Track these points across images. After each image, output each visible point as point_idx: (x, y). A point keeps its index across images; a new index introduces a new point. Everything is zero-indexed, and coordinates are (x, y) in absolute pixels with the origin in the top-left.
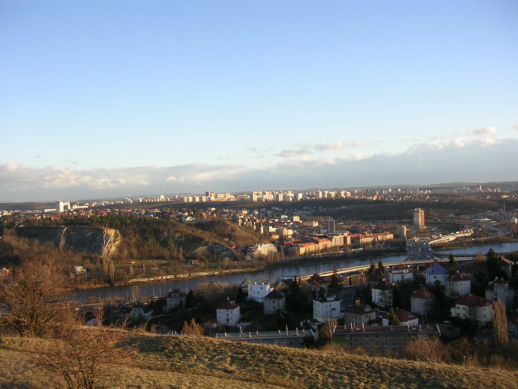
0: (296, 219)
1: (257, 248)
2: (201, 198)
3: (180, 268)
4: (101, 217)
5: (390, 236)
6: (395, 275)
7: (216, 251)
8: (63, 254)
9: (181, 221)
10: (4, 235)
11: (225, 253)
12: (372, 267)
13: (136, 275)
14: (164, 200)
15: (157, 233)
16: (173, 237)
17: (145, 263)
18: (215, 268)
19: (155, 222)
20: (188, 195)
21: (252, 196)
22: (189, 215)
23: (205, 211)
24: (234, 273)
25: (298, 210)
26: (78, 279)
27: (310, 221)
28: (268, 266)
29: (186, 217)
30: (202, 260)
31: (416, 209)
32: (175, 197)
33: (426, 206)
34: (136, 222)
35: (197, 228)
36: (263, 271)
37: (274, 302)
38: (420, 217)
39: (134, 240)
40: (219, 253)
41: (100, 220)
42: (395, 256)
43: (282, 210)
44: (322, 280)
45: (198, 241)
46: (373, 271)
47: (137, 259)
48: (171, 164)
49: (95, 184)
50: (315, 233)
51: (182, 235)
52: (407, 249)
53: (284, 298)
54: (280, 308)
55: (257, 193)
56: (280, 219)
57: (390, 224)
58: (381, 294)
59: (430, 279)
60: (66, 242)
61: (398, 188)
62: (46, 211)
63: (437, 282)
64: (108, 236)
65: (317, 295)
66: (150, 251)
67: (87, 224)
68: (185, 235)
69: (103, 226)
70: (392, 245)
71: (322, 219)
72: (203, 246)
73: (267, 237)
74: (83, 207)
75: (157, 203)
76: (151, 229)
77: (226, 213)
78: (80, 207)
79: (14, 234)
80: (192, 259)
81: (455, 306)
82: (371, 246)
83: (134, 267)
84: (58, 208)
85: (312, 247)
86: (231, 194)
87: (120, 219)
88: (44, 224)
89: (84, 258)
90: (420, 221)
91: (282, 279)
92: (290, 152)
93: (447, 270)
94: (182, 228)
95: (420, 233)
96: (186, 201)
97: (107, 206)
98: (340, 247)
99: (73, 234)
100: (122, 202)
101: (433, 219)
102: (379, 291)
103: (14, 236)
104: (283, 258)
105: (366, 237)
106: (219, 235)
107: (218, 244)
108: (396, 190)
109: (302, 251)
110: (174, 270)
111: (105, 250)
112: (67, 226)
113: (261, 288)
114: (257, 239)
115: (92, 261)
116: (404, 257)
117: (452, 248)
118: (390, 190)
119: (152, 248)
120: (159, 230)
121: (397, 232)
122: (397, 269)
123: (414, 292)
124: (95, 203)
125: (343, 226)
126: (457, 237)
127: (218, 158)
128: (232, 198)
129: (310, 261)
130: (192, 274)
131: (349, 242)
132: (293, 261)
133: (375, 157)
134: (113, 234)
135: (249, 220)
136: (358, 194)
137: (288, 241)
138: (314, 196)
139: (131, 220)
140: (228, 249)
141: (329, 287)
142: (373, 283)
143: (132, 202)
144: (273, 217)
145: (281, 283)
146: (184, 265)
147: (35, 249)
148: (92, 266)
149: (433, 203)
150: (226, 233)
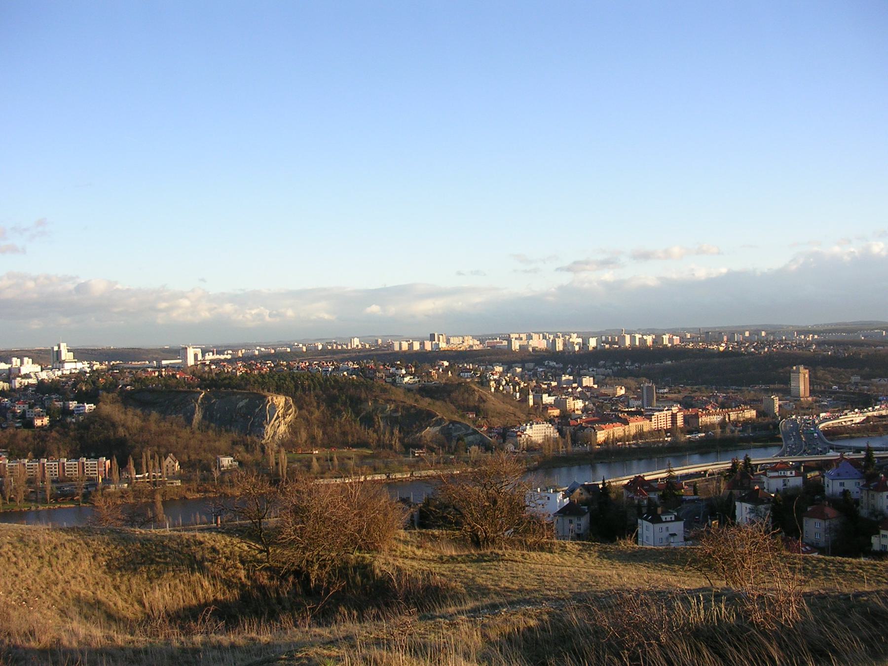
0: (588, 381)
1: (525, 430)
2: (422, 344)
3: (396, 463)
4: (260, 374)
5: (751, 414)
6: (772, 481)
7: (455, 434)
8: (199, 436)
9: (394, 383)
10: (101, 403)
11: (471, 438)
12: (735, 465)
13: (323, 473)
14: (360, 347)
15: (355, 403)
16: (383, 410)
17: (336, 453)
19: (353, 384)
20: (400, 339)
21: (510, 342)
22: (408, 374)
23: (433, 367)
25: (590, 367)
26: (227, 478)
27: (612, 385)
28: (544, 462)
29: (403, 377)
30: (431, 450)
32: (377, 341)
33: (811, 362)
34: (320, 384)
35: (422, 396)
36: (536, 469)
37: (571, 522)
38: (802, 381)
39: (317, 414)
40: (460, 439)
41: (260, 380)
42: (761, 447)
43: (561, 365)
44: (651, 486)
45: (426, 417)
46: (735, 472)
47: (323, 446)
48: (375, 284)
49: (241, 317)
50: (621, 407)
51: (397, 407)
52: (781, 436)
53: (588, 515)
54: (581, 532)
55: (517, 336)
56: (559, 382)
57: (750, 393)
58: (752, 511)
59: (833, 487)
60: (204, 417)
61: (760, 331)
62: (164, 362)
63: (845, 493)
64: (274, 407)
65: (644, 510)
66: (344, 434)
67: (238, 386)
69: (266, 390)
70: (754, 428)
71: (632, 382)
72: (434, 425)
73: (539, 413)
74: (222, 357)
75: (348, 351)
76: (347, 396)
77: (469, 371)
78: (218, 357)
79: (118, 401)
80: (414, 448)
81: (878, 533)
82: (719, 430)
83: (318, 459)
84: (185, 358)
85: (618, 430)
86: (474, 337)
87: (293, 378)
88: (166, 385)
89: (234, 443)
90: (802, 387)
91: (581, 483)
92: (587, 263)
93: (862, 473)
94: (399, 395)
95: (802, 409)
96: (397, 348)
97: (265, 357)
98: (667, 431)
99: (214, 403)
100: (289, 350)
101: (824, 384)
102: (749, 506)
103: (117, 404)
104: (570, 448)
105: (709, 414)
106: (459, 407)
107: (459, 423)
108: (757, 332)
109: (601, 436)
110: (386, 466)
111: (269, 430)
112: (205, 388)
114: (523, 417)
115: (248, 448)
116: (775, 451)
117: (858, 435)
118: (747, 334)
119: (348, 427)
120: (359, 398)
121: (762, 407)
122: (775, 468)
123: (809, 509)
124: (243, 351)
125: (669, 396)
126: (868, 417)
127: (459, 273)
128: (477, 345)
129: (616, 454)
130: (417, 474)
131: (680, 422)
132: (587, 453)
133: (730, 275)
134: (282, 404)
135: (507, 383)
136: (692, 340)
137: (576, 419)
138: (616, 343)
139: (312, 380)
140: (475, 432)
141: (660, 497)
142: (735, 492)
143: (304, 349)
144: (547, 379)
145: (578, 490)
146: (401, 458)
147: (153, 427)
148: (248, 457)
149: (824, 357)
150: (471, 404)
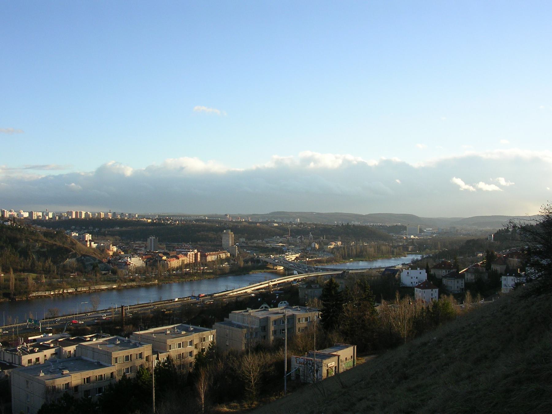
16: (34, 247)
18: (115, 281)
24: (132, 287)
31: (225, 231)
37: (458, 282)
51: (43, 244)
68: (47, 245)
72: (71, 258)
113: (420, 273)
